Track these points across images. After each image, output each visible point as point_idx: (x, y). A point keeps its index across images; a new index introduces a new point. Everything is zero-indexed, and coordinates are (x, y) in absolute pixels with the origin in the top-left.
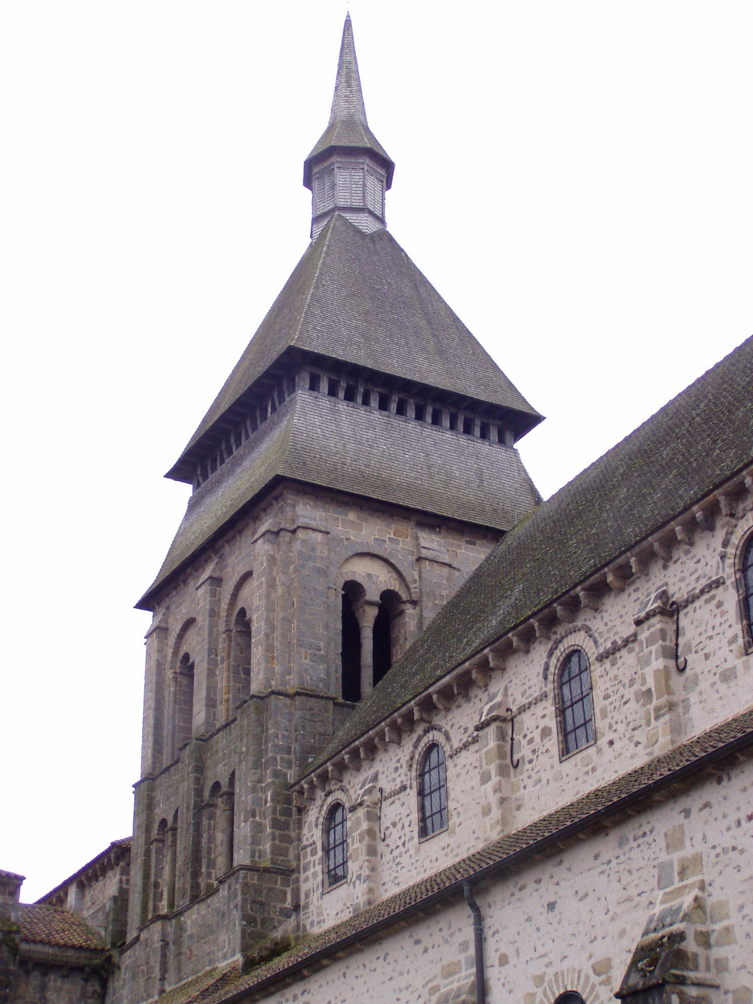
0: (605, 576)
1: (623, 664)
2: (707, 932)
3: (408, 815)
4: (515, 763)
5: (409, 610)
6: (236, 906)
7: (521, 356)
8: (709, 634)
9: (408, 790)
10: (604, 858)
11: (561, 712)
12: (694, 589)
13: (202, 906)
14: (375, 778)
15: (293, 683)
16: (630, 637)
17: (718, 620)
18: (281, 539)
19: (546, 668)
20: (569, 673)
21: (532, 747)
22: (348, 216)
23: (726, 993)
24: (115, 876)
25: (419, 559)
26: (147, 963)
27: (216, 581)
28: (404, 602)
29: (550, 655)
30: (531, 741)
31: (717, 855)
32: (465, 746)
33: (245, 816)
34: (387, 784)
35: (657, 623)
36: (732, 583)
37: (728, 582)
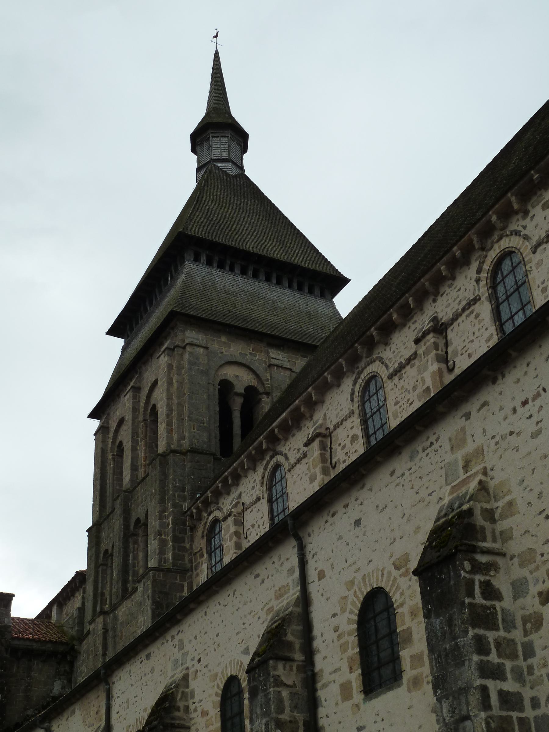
0: (391, 316)
1: (408, 377)
2: (492, 509)
3: (262, 517)
4: (333, 465)
5: (265, 399)
6: (148, 597)
7: (336, 253)
8: (471, 339)
9: (262, 500)
10: (398, 473)
11: (364, 422)
12: (458, 309)
13: (129, 601)
14: (240, 496)
15: (186, 444)
16: (411, 355)
17: (478, 326)
18: (176, 353)
19: (353, 393)
20: (369, 393)
21: (345, 451)
22: (219, 165)
23: (512, 558)
24: (80, 594)
25: (270, 366)
26: (95, 645)
27: (137, 390)
28: (261, 394)
29: (355, 383)
30: (344, 447)
31: (497, 443)
32: (299, 461)
33: (154, 535)
34: (247, 499)
35: (431, 339)
36: (486, 298)
37: (483, 298)
